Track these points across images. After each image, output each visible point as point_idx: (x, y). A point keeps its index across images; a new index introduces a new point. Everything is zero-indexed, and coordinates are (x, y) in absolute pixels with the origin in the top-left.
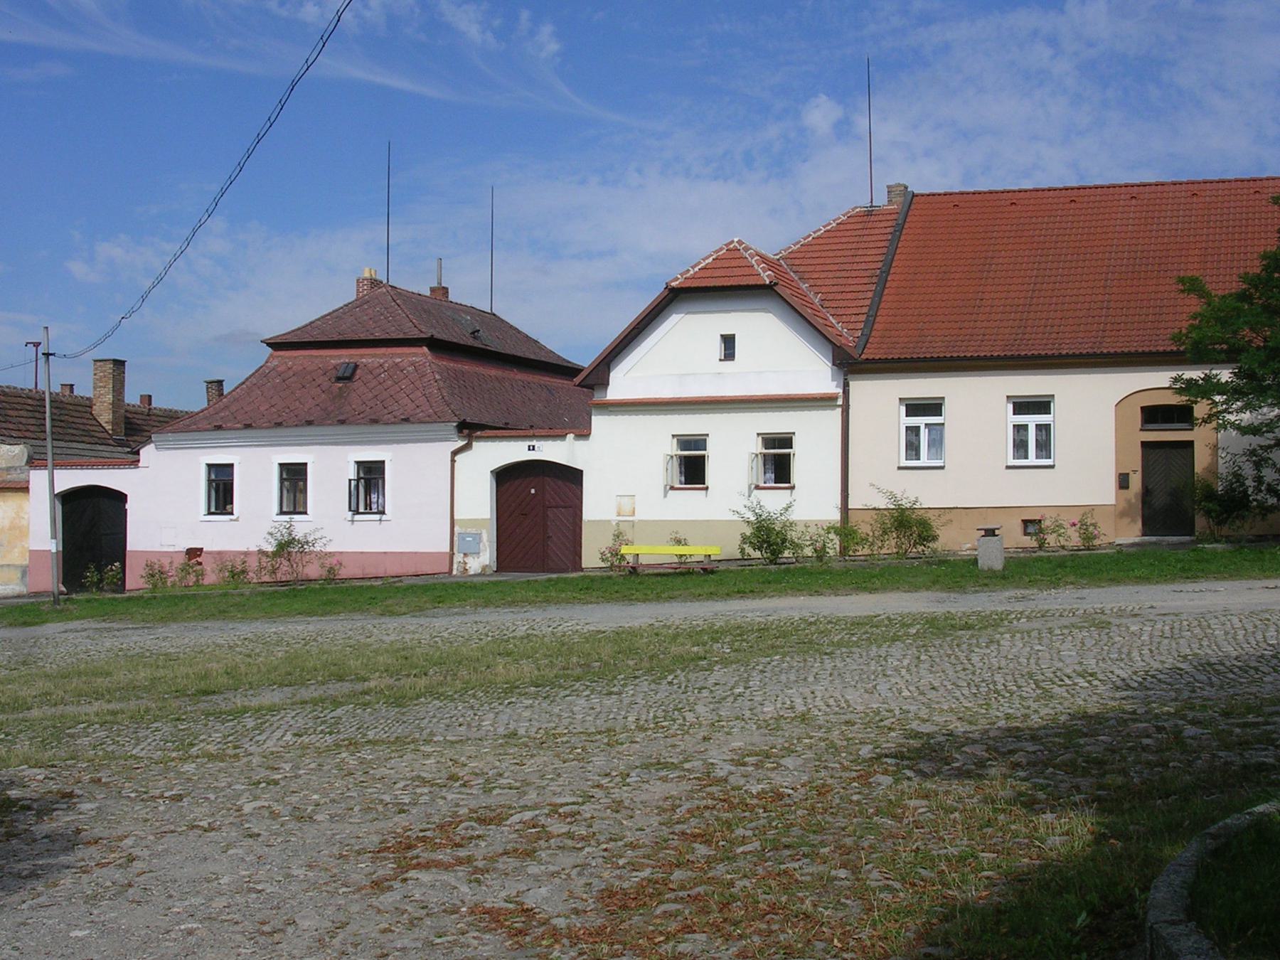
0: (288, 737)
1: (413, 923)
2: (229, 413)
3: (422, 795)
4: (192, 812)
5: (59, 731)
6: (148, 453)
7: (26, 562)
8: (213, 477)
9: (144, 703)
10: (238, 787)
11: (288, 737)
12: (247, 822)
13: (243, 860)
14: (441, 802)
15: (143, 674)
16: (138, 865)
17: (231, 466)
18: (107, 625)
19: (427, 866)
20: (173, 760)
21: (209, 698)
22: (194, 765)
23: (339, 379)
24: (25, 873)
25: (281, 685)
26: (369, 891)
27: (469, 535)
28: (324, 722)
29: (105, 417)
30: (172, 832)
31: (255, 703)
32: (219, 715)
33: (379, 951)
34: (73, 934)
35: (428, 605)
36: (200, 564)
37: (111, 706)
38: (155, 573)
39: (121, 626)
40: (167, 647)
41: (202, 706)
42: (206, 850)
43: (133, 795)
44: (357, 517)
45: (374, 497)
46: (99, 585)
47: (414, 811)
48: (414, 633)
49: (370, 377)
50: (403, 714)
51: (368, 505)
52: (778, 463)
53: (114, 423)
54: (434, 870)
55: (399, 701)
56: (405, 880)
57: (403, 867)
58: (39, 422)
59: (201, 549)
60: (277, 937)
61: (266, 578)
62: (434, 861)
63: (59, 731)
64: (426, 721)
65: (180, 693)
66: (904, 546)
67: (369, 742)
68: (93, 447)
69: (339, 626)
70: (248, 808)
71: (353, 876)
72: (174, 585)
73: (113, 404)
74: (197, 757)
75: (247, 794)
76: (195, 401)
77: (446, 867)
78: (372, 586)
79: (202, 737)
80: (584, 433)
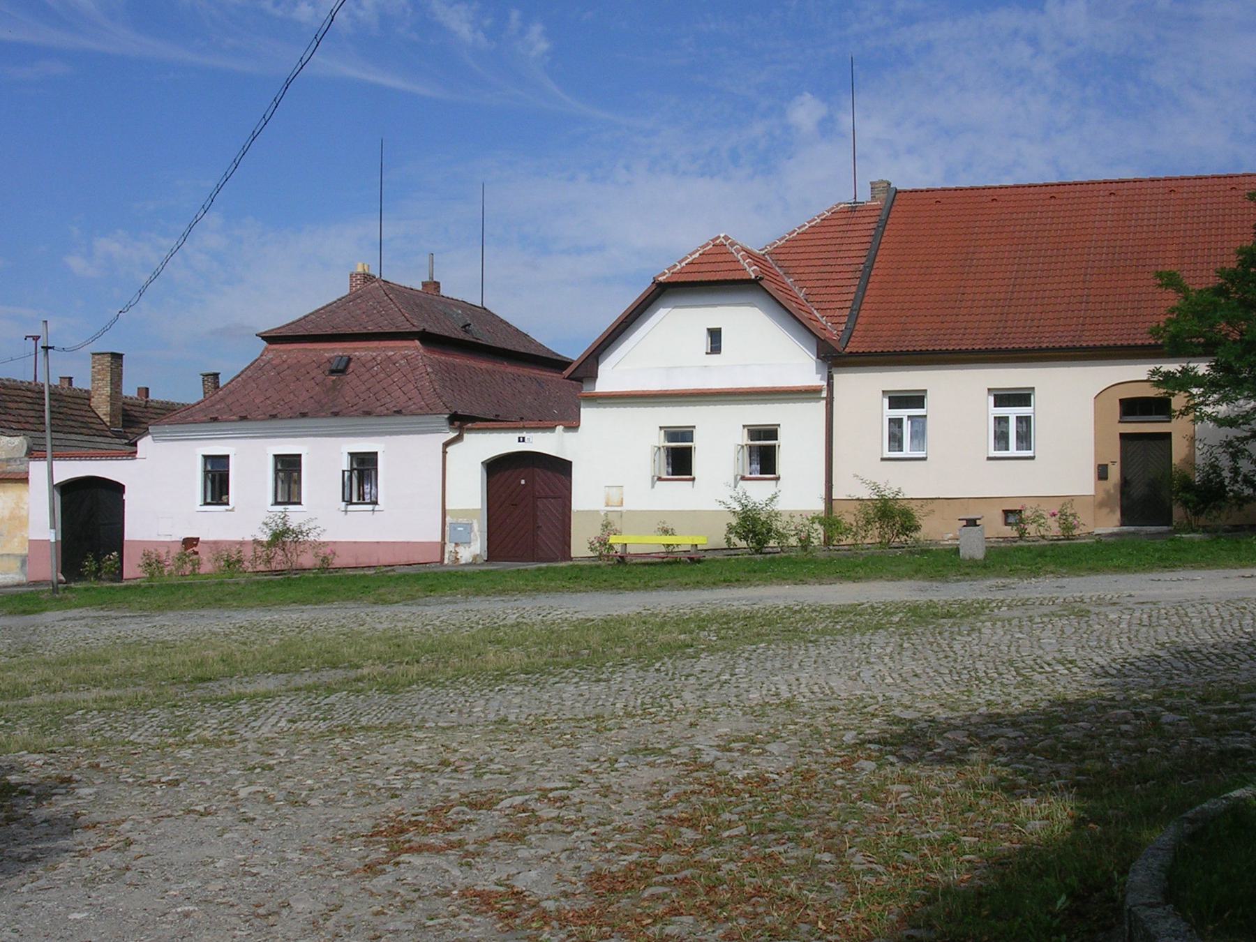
0: (283, 723)
1: (405, 906)
2: (225, 405)
3: (414, 780)
4: (188, 796)
5: (58, 718)
6: (145, 444)
7: (26, 552)
8: (209, 468)
9: (141, 690)
10: (233, 772)
11: (283, 723)
12: (243, 806)
13: (238, 843)
14: (433, 787)
15: (141, 662)
16: (136, 849)
17: (227, 457)
18: (105, 614)
19: (419, 850)
20: (170, 745)
21: (205, 685)
22: (190, 751)
23: (333, 372)
24: (24, 857)
25: (276, 672)
26: (363, 874)
27: (461, 525)
28: (318, 709)
29: (103, 409)
30: (169, 816)
31: (250, 689)
32: (215, 702)
33: (372, 933)
34: (71, 917)
35: (420, 594)
36: (196, 553)
37: (109, 693)
38: (153, 562)
39: (118, 614)
40: (163, 635)
41: (198, 693)
42: (203, 834)
43: (130, 780)
44: (351, 508)
45: (367, 488)
46: (97, 575)
47: (406, 796)
48: (406, 621)
49: (363, 369)
50: (396, 701)
51: (361, 496)
52: (763, 454)
53: (112, 415)
54: (426, 854)
55: (391, 687)
56: (398, 863)
57: (395, 851)
58: (38, 414)
59: (198, 539)
60: (272, 919)
61: (261, 568)
62: (425, 845)
63: (58, 718)
64: (418, 707)
65: (177, 680)
66: (887, 536)
67: (362, 728)
68: (92, 439)
69: (332, 614)
70: (243, 793)
71: (347, 859)
72: (170, 574)
73: (111, 396)
74: (194, 743)
75: (242, 779)
76: (192, 393)
77: (438, 851)
78: (365, 575)
79: (198, 723)
80: (573, 425)
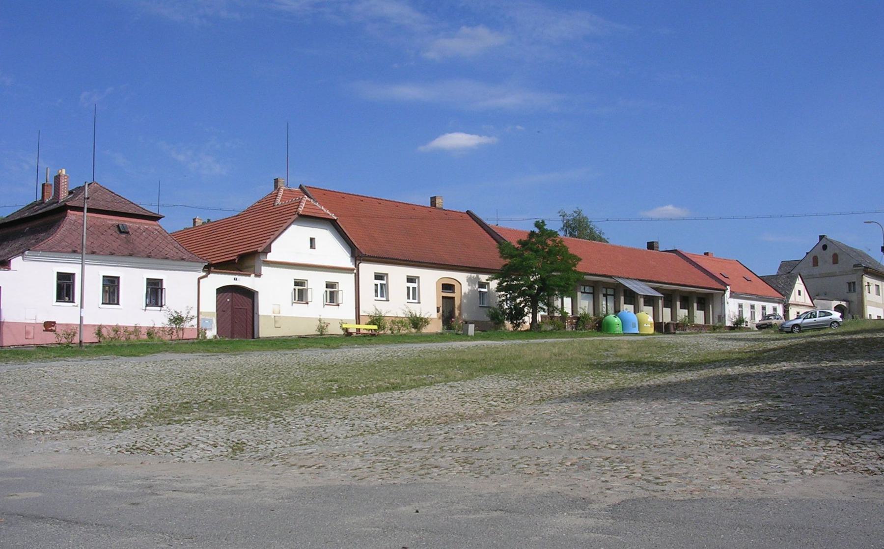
66: (379, 331)
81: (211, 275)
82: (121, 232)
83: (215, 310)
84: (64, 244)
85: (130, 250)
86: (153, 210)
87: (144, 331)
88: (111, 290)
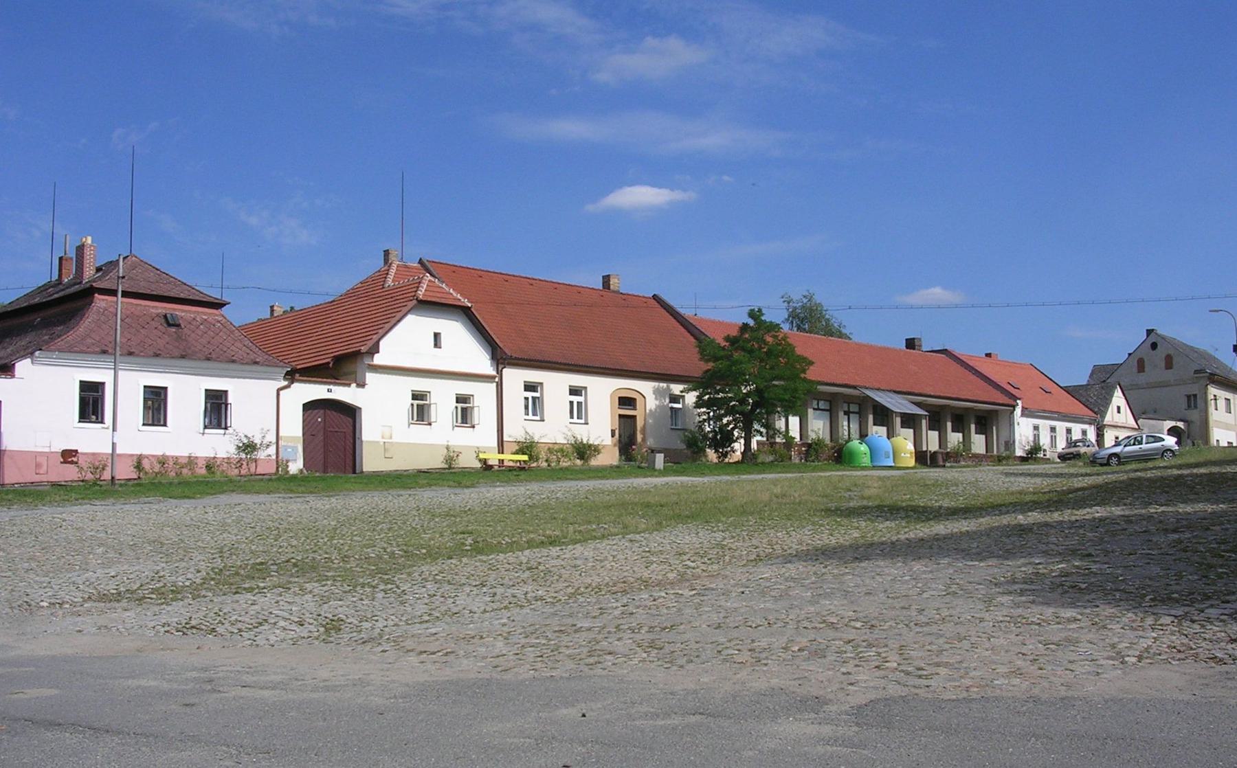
52: (465, 415)
66: (530, 463)
81: (296, 385)
82: (169, 325)
83: (301, 434)
84: (89, 341)
85: (182, 350)
86: (215, 294)
87: (202, 463)
88: (156, 405)
